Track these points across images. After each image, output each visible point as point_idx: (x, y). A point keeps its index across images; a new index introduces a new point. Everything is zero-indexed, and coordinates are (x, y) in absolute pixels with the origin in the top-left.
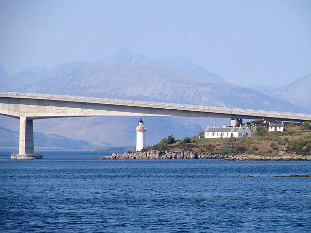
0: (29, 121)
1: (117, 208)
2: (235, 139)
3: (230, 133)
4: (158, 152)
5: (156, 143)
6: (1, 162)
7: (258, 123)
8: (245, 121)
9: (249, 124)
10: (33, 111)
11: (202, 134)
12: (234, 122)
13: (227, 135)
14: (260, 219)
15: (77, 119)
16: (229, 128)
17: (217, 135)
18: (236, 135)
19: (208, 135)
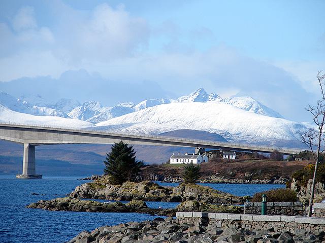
0: (31, 147)
3: (190, 160)
7: (214, 152)
10: (36, 139)
12: (197, 151)
17: (181, 161)
18: (195, 161)
19: (173, 161)
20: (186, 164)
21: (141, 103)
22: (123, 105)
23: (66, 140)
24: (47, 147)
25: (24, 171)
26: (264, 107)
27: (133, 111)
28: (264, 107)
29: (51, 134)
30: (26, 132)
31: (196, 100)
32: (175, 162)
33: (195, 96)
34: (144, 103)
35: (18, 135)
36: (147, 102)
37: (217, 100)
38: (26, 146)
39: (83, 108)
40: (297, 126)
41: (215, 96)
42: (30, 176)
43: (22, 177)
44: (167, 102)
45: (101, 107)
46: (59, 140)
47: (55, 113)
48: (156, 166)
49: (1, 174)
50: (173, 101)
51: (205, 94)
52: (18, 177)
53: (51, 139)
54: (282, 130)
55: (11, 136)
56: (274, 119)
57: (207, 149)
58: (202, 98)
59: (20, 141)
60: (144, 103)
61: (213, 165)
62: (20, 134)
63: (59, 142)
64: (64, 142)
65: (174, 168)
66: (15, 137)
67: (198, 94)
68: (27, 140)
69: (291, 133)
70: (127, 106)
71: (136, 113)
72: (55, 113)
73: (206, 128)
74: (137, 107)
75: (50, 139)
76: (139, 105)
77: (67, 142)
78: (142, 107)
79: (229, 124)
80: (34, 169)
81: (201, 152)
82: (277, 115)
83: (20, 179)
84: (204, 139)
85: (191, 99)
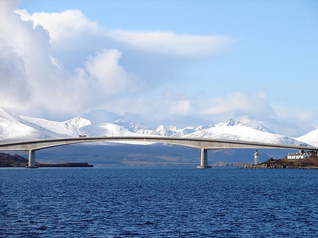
0: (205, 151)
1: (103, 212)
2: (302, 159)
3: (299, 156)
4: (266, 165)
5: (265, 161)
6: (317, 219)
7: (312, 152)
8: (305, 151)
9: (308, 152)
10: (208, 146)
11: (286, 158)
12: (300, 152)
13: (298, 157)
14: (305, 219)
15: (40, 138)
16: (299, 154)
17: (294, 157)
18: (302, 157)
19: (289, 157)
20: (219, 170)
23: (226, 146)
24: (217, 150)
26: (265, 128)
28: (265, 128)
29: (217, 143)
31: (228, 125)
32: (290, 158)
33: (228, 123)
34: (201, 127)
35: (198, 144)
36: (202, 126)
37: (240, 124)
38: (203, 150)
39: (167, 130)
40: (286, 138)
41: (239, 122)
47: (153, 133)
48: (280, 160)
49: (313, 151)
52: (198, 167)
54: (277, 141)
56: (271, 135)
57: (305, 151)
58: (232, 123)
59: (199, 147)
60: (201, 127)
61: (312, 159)
65: (291, 161)
66: (196, 145)
68: (202, 147)
69: (282, 142)
72: (153, 133)
73: (251, 141)
74: (197, 129)
75: (216, 146)
76: (198, 128)
77: (24, 149)
79: (249, 137)
81: (303, 152)
82: (273, 133)
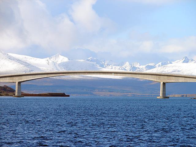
0: (164, 84)
10: (166, 80)
21: (159, 64)
22: (150, 64)
25: (161, 95)
27: (155, 68)
29: (174, 77)
30: (161, 77)
31: (183, 62)
33: (183, 60)
34: (160, 63)
35: (158, 78)
36: (161, 63)
37: (193, 62)
38: (162, 83)
39: (132, 66)
41: (192, 60)
42: (164, 97)
43: (160, 98)
44: (171, 63)
45: (140, 65)
46: (177, 80)
47: (120, 69)
50: (173, 62)
51: (188, 59)
52: (158, 98)
53: (174, 80)
55: (154, 78)
58: (186, 61)
59: (159, 81)
60: (160, 63)
62: (159, 78)
63: (177, 81)
64: (180, 81)
66: (157, 79)
67: (184, 59)
68: (162, 80)
70: (152, 65)
71: (157, 68)
72: (120, 69)
74: (157, 65)
75: (173, 80)
76: (158, 64)
78: (159, 66)
80: (165, 94)
83: (159, 99)
84: (28, 96)
85: (181, 61)
